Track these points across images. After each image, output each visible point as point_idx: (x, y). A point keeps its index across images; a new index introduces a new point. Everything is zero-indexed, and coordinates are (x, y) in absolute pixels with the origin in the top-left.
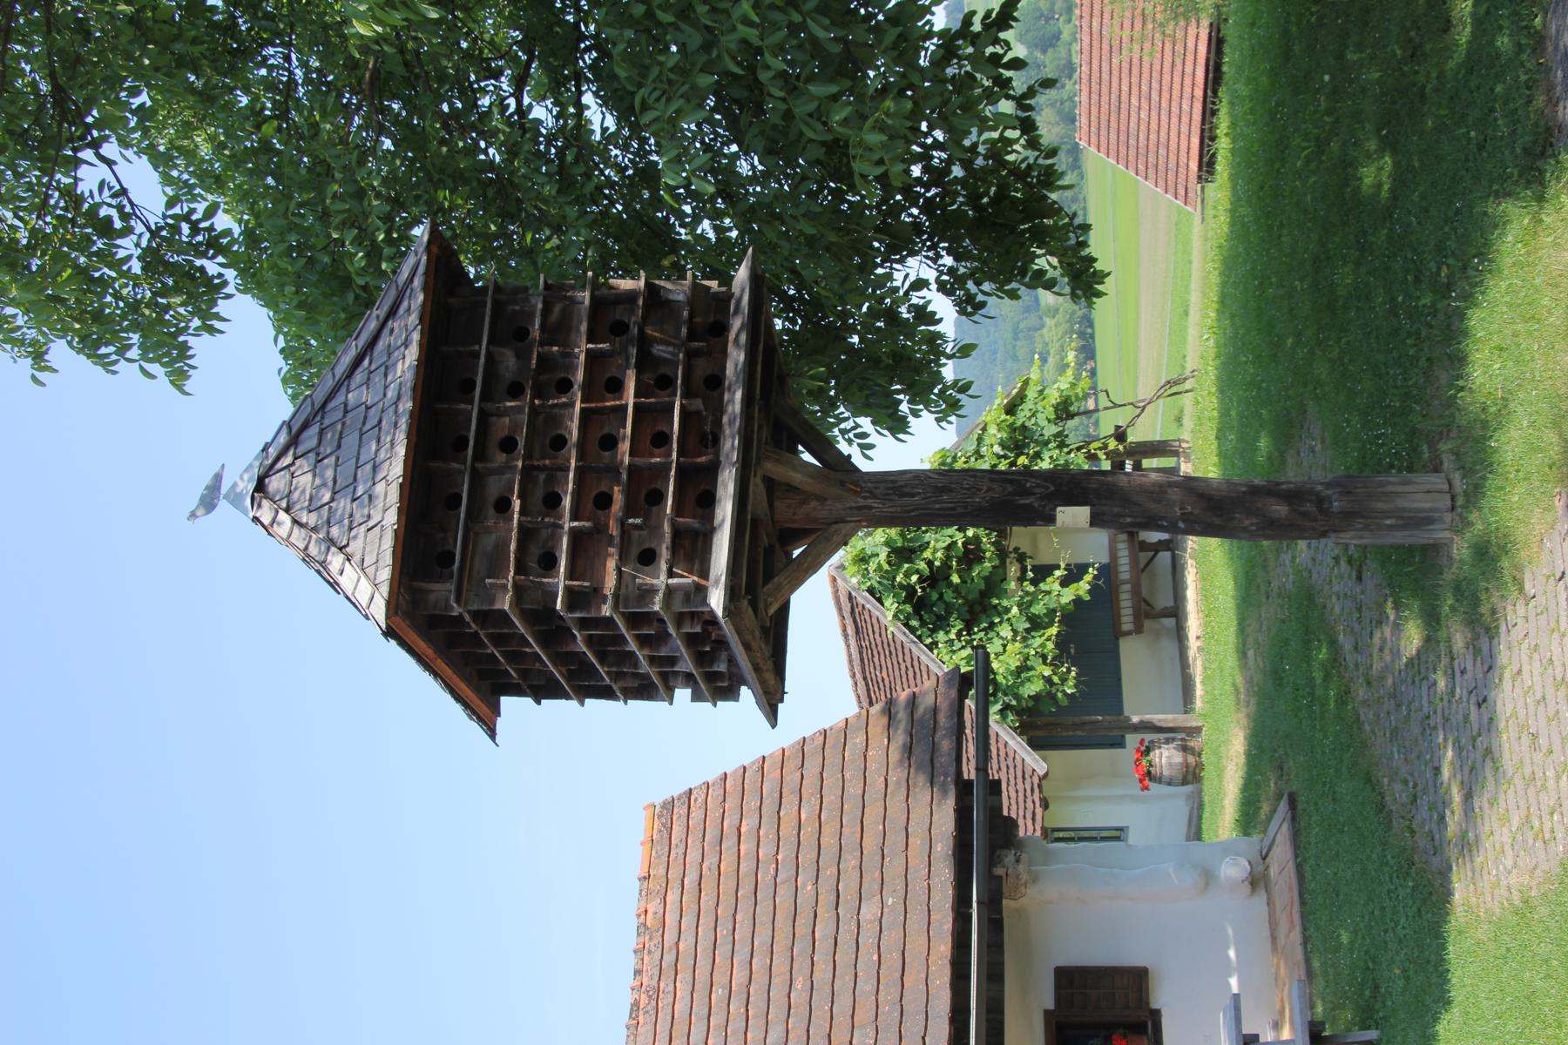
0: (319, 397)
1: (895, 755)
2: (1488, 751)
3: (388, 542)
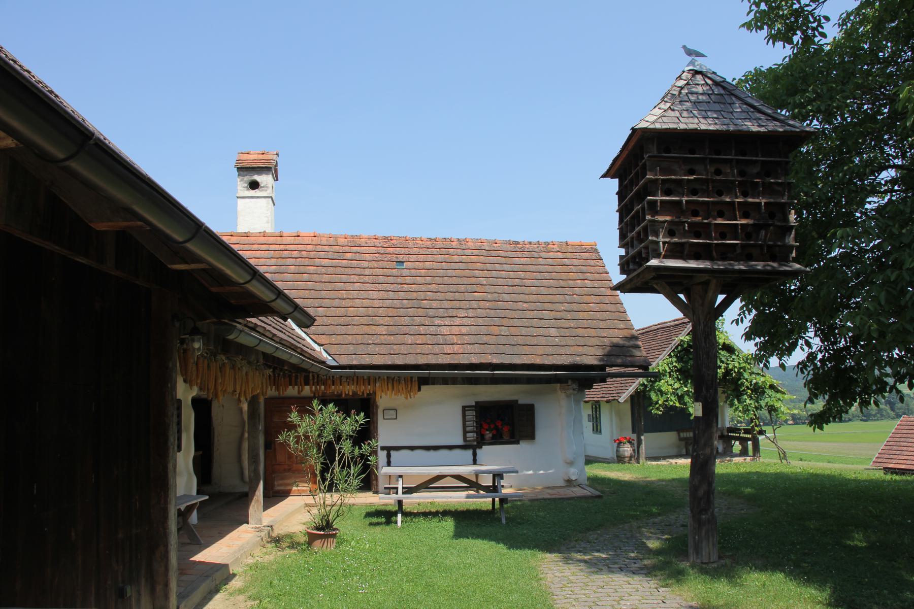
0: (736, 92)
1: (615, 340)
2: (601, 570)
3: (672, 126)
